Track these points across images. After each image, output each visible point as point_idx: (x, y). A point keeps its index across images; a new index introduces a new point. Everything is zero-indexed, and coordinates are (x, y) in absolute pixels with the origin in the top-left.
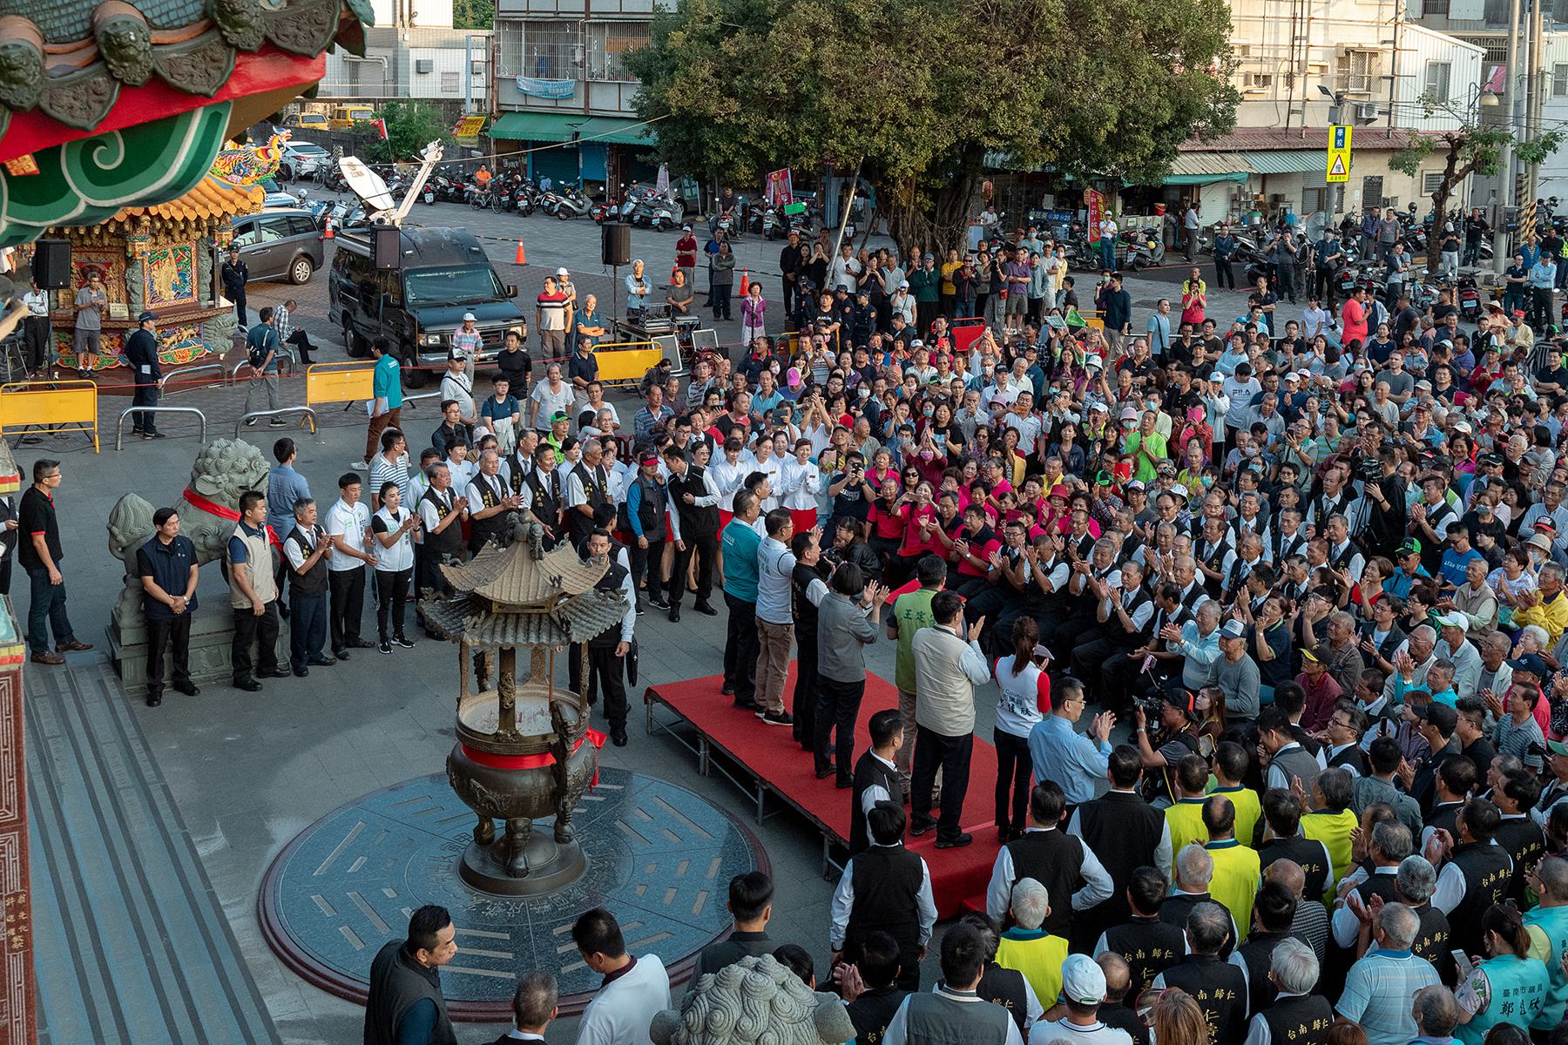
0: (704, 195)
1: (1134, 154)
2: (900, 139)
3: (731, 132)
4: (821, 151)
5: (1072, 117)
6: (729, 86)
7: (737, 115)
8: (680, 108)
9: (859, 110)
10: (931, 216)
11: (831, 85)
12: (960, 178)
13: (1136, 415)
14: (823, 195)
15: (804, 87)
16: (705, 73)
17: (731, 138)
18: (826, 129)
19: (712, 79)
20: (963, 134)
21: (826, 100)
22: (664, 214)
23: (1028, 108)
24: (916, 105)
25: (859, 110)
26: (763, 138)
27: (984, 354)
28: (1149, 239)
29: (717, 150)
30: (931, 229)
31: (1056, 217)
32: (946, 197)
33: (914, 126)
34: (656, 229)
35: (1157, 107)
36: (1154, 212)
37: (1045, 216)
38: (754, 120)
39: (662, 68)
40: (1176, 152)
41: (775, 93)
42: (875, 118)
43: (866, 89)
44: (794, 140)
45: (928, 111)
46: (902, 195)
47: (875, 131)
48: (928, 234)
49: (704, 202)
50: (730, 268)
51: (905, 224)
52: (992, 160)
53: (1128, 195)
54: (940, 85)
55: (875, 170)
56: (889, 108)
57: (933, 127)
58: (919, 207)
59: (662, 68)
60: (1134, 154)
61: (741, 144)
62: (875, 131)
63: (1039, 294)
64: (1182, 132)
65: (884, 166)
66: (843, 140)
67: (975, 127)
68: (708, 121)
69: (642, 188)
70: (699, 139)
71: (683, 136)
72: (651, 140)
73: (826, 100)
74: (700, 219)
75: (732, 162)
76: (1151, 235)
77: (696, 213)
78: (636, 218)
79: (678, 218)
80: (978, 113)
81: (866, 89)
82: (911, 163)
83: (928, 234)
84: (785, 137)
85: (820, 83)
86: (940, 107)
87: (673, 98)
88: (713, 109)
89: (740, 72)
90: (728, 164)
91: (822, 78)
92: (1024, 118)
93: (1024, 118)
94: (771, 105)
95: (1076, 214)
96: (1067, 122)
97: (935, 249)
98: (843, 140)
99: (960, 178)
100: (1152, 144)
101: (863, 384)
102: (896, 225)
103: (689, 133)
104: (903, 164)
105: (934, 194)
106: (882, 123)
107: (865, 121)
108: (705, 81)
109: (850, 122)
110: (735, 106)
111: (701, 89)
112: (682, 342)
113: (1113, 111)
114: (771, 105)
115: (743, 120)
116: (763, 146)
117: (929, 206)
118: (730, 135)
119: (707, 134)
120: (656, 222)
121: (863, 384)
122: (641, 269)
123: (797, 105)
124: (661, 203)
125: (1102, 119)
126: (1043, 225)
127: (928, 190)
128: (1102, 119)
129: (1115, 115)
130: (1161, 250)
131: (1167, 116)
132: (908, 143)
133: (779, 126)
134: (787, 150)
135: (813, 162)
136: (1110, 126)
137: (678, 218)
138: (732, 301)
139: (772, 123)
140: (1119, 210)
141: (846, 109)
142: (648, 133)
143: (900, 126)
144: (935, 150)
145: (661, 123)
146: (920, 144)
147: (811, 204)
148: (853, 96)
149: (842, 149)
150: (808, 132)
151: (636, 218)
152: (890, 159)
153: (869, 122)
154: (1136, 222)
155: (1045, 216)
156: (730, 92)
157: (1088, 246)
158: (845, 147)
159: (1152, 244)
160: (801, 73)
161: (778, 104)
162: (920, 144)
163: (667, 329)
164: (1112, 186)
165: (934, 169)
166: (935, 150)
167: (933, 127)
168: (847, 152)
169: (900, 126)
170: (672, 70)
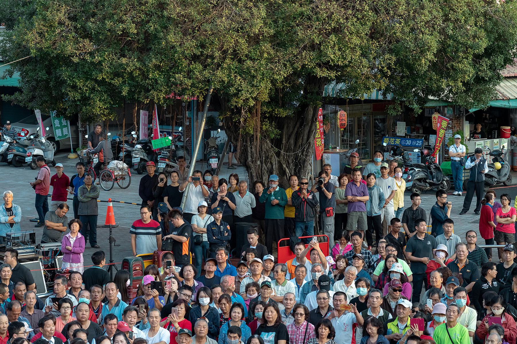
0: (76, 132)
1: (455, 80)
2: (240, 72)
3: (87, 70)
4: (168, 83)
5: (394, 46)
6: (84, 28)
7: (91, 54)
8: (40, 50)
9: (203, 46)
10: (277, 143)
11: (177, 25)
12: (304, 107)
13: (442, 307)
14: (189, 130)
15: (152, 27)
16: (61, 16)
17: (87, 76)
18: (175, 67)
19: (67, 22)
20: (298, 65)
21: (171, 38)
22: (37, 152)
23: (356, 40)
24: (255, 40)
25: (203, 46)
26: (117, 75)
27: (314, 262)
28: (495, 160)
29: (74, 87)
30: (278, 154)
31: (409, 142)
32: (291, 125)
33: (253, 60)
34: (30, 166)
35: (474, 37)
36: (501, 135)
37: (398, 141)
38: (107, 58)
39: (22, 14)
40: (499, 78)
41: (125, 33)
42: (217, 54)
43: (208, 27)
44: (145, 77)
45: (266, 46)
46: (253, 125)
47: (219, 65)
48: (275, 160)
49: (76, 139)
50: (95, 198)
51: (253, 150)
52: (332, 89)
53: (475, 119)
54: (275, 22)
55: (220, 101)
56: (230, 43)
57: (270, 60)
58: (265, 135)
59: (22, 14)
60: (455, 80)
61: (96, 81)
62: (219, 65)
63: (376, 211)
64: (500, 59)
65: (228, 97)
66: (189, 74)
67: (308, 59)
68: (66, 60)
69: (17, 128)
70: (57, 78)
71: (42, 75)
72: (15, 80)
73: (171, 38)
74: (72, 156)
75: (88, 98)
76: (497, 156)
77: (68, 151)
78: (10, 157)
79: (50, 156)
80: (313, 47)
81: (208, 27)
82: (253, 93)
83: (275, 160)
84: (136, 73)
85: (166, 23)
86: (279, 42)
87: (32, 40)
88: (70, 49)
89: (94, 15)
90: (85, 100)
91: (169, 18)
92: (353, 50)
93: (353, 50)
94: (123, 44)
95: (427, 139)
96: (391, 51)
97: (282, 173)
98: (189, 74)
99: (304, 107)
100: (471, 72)
101: (202, 294)
102: (245, 152)
103: (49, 73)
104: (245, 95)
105: (280, 123)
106: (224, 58)
107: (207, 57)
108: (61, 23)
109: (195, 58)
110: (89, 45)
111: (58, 31)
112: (46, 267)
113: (433, 42)
114: (123, 44)
115: (97, 59)
116: (117, 82)
117: (274, 132)
118: (86, 73)
119: (65, 73)
120: (29, 159)
121: (202, 294)
122: (10, 200)
123: (146, 44)
124: (34, 142)
125: (423, 50)
126: (396, 151)
127: (272, 118)
128: (423, 50)
129: (435, 46)
130: (507, 170)
131: (484, 44)
132: (249, 76)
133: (130, 63)
134: (138, 85)
135: (162, 96)
136: (430, 56)
137: (50, 156)
138: (98, 231)
139: (124, 60)
140: (467, 133)
141: (190, 45)
142: (11, 74)
143: (240, 61)
144: (273, 82)
145: (23, 63)
146: (259, 77)
147: (177, 139)
148: (197, 34)
149: (189, 82)
150: (157, 67)
151: (10, 157)
152: (232, 90)
153: (212, 57)
154: (485, 144)
155: (398, 141)
156: (86, 34)
157: (437, 168)
158: (190, 81)
159: (498, 165)
160: (149, 15)
161: (129, 43)
162: (259, 77)
163: (32, 255)
164: (459, 114)
165: (278, 98)
166: (273, 82)
167: (270, 60)
168: (193, 85)
169: (240, 61)
170: (32, 14)
